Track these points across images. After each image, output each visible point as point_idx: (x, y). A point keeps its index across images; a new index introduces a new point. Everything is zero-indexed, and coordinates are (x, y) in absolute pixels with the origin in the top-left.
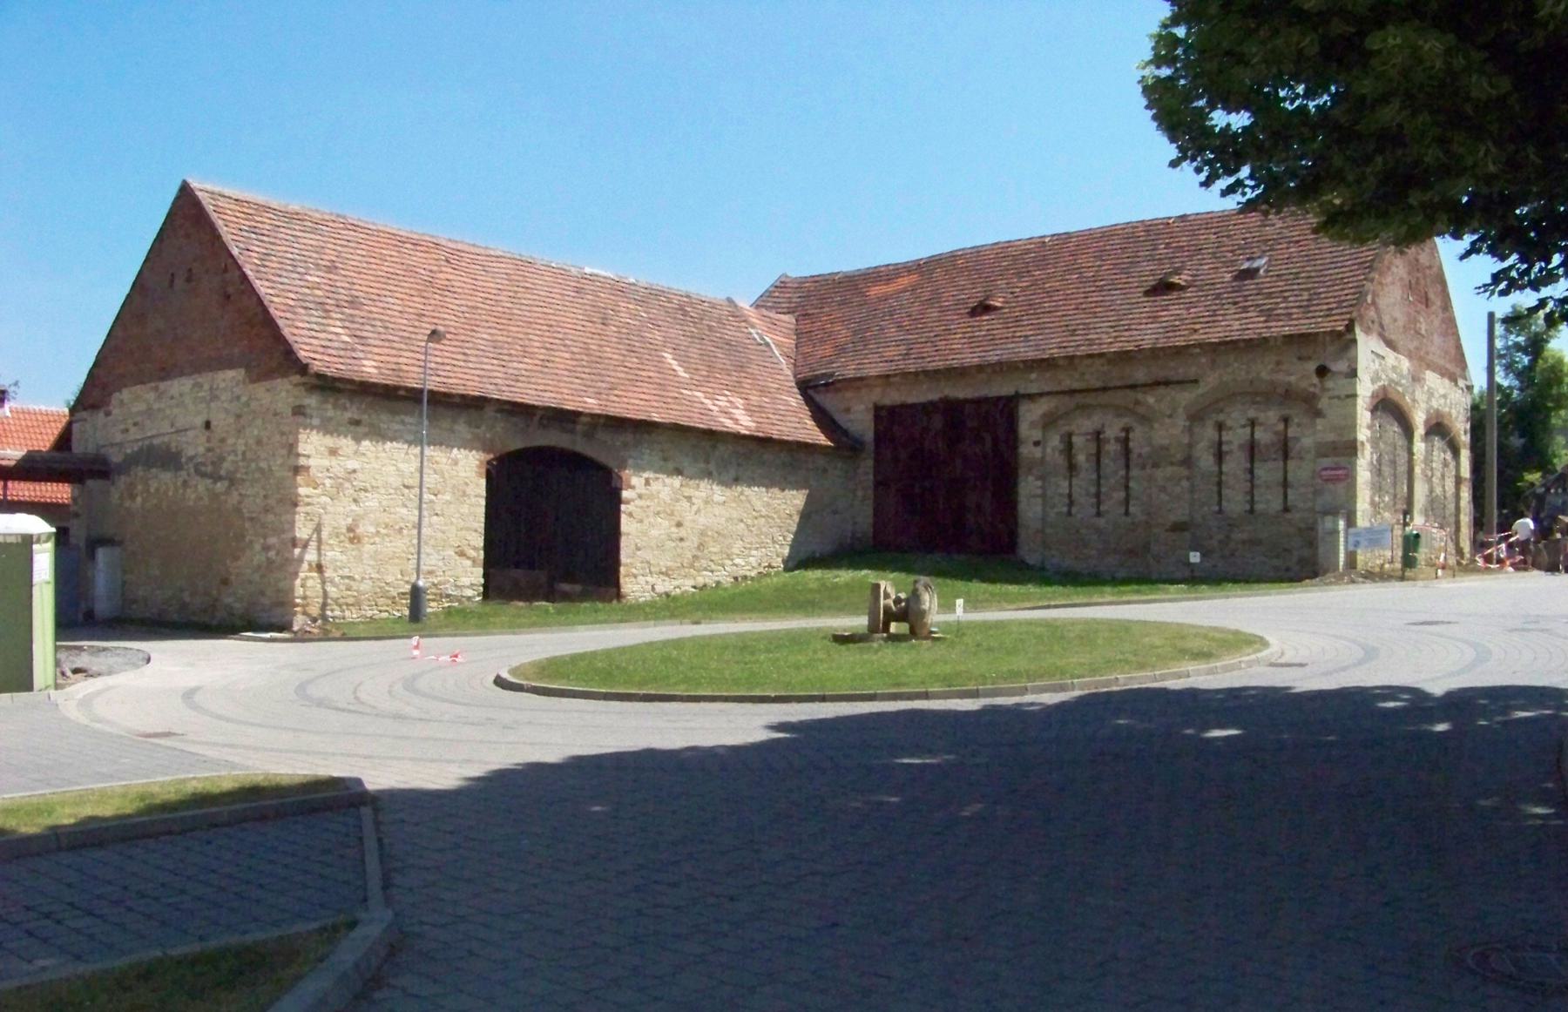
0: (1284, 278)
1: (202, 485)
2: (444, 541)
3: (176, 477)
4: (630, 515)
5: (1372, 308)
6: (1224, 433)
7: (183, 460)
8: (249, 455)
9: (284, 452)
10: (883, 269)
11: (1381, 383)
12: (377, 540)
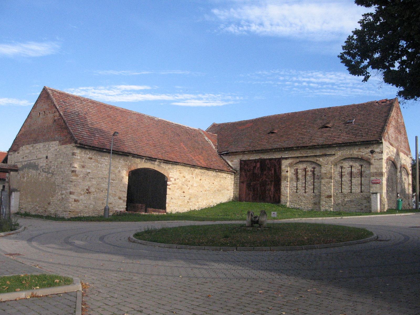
0: (360, 125)
1: (44, 175)
3: (37, 172)
4: (170, 189)
5: (387, 133)
6: (343, 169)
7: (39, 167)
9: (69, 166)
11: (389, 156)
12: (95, 193)
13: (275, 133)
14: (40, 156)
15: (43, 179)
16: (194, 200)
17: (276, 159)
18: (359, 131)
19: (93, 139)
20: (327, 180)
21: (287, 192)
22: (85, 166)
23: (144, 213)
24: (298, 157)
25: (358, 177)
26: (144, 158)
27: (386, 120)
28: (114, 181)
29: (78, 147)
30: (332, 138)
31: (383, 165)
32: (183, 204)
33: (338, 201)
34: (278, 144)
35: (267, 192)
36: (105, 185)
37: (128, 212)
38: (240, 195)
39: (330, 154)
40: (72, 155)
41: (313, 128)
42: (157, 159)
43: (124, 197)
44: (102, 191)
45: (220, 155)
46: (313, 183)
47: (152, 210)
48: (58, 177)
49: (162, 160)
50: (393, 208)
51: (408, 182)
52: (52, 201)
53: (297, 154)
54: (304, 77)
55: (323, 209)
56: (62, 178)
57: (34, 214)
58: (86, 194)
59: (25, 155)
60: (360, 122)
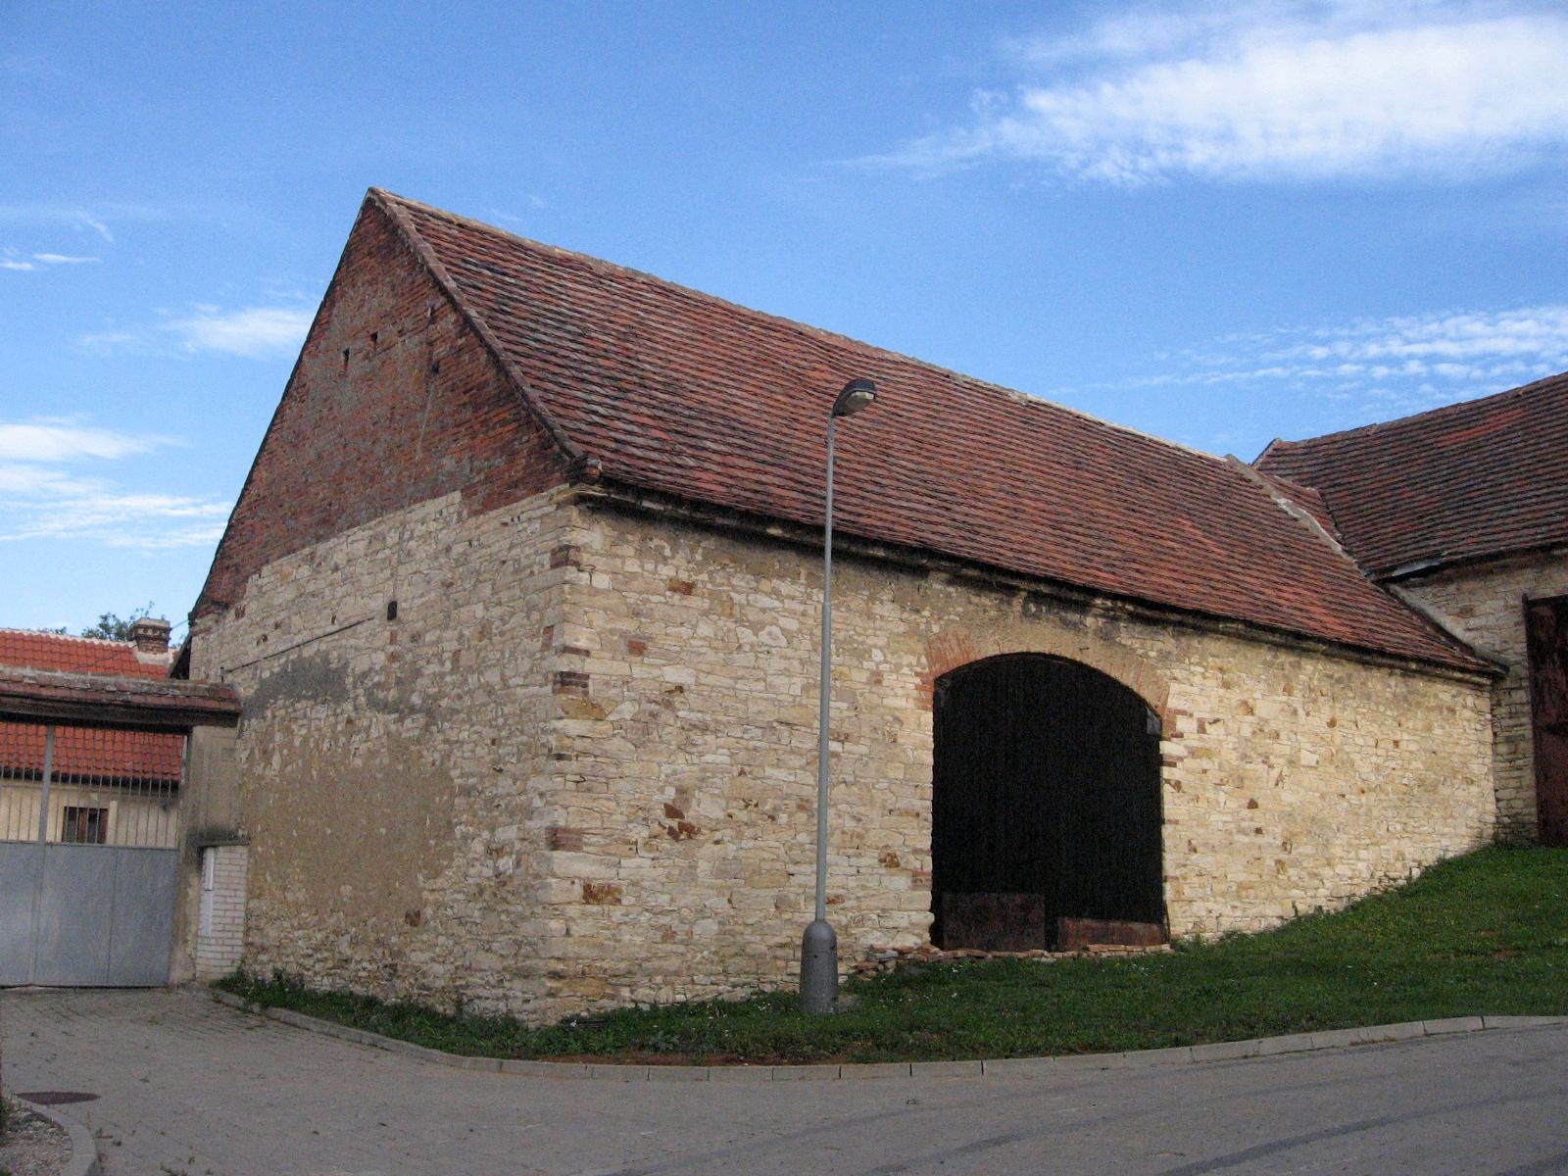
1: (379, 723)
2: (860, 836)
3: (336, 715)
4: (1178, 786)
8: (466, 658)
9: (537, 644)
10: (1452, 411)
14: (351, 609)
15: (372, 754)
16: (1309, 850)
19: (691, 462)
22: (650, 639)
23: (1048, 958)
26: (1023, 585)
28: (847, 745)
29: (595, 507)
32: (1254, 878)
36: (791, 776)
37: (950, 953)
38: (1543, 805)
40: (554, 566)
42: (1094, 592)
43: (916, 851)
44: (773, 818)
47: (1087, 928)
48: (465, 735)
49: (1125, 598)
52: (431, 897)
54: (1408, 342)
56: (493, 734)
57: (323, 984)
58: (666, 843)
59: (271, 621)
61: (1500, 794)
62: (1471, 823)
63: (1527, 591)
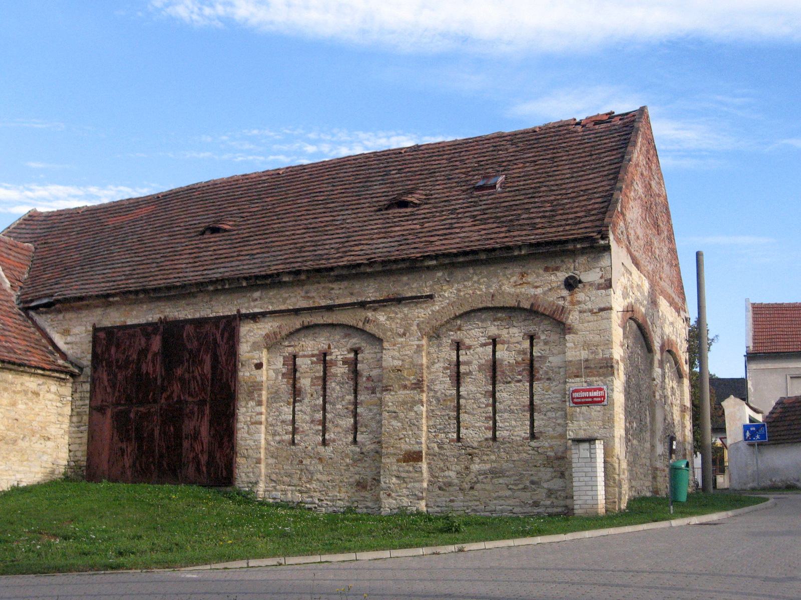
5: (621, 217)
6: (462, 352)
11: (629, 300)
13: (225, 231)
17: (218, 319)
18: (519, 212)
20: (402, 394)
21: (259, 441)
24: (296, 312)
25: (519, 381)
27: (618, 173)
30: (424, 239)
31: (614, 332)
33: (446, 473)
34: (229, 265)
35: (186, 444)
38: (90, 455)
39: (414, 294)
41: (356, 211)
45: (26, 310)
46: (351, 407)
50: (643, 494)
51: (682, 400)
53: (295, 299)
55: (388, 505)
60: (522, 183)
61: (71, 448)
62: (44, 465)
63: (96, 322)
